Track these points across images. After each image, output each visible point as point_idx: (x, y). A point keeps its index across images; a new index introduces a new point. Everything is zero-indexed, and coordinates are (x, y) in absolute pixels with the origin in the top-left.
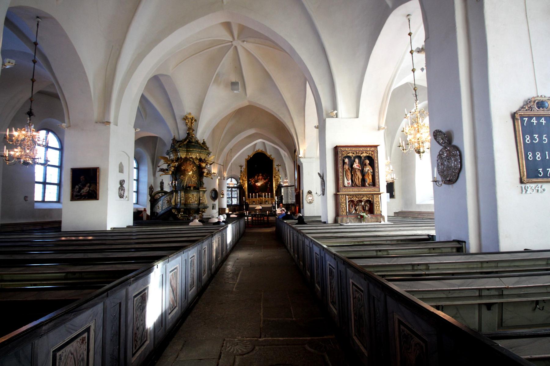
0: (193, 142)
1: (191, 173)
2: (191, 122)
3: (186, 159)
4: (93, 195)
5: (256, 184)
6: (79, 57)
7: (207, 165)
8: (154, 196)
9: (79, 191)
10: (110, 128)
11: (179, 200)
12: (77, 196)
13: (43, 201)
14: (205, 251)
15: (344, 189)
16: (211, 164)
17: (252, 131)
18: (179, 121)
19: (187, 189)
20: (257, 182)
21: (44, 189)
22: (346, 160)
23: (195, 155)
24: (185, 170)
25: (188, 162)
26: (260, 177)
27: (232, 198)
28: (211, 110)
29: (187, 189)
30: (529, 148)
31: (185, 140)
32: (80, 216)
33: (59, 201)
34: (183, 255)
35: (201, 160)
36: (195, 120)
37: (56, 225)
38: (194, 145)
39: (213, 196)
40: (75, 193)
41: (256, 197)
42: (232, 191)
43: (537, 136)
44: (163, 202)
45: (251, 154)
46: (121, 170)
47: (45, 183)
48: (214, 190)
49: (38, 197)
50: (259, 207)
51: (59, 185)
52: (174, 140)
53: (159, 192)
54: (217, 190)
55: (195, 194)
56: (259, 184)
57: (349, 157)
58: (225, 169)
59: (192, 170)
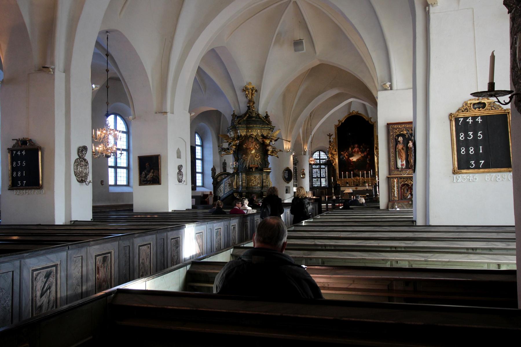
0: (253, 117)
1: (253, 152)
2: (251, 93)
3: (247, 137)
4: (156, 180)
5: (351, 159)
6: (139, 57)
7: (271, 141)
8: (217, 178)
9: (145, 177)
10: (166, 118)
11: (240, 183)
12: (144, 181)
13: (116, 185)
14: (234, 228)
15: (396, 172)
16: (276, 140)
17: (335, 92)
18: (239, 93)
19: (248, 171)
20: (352, 156)
21: (116, 173)
22: (400, 139)
23: (256, 132)
24: (247, 149)
25: (250, 140)
26: (356, 149)
27: (321, 178)
28: (274, 78)
29: (248, 171)
30: (466, 144)
31: (245, 114)
32: (145, 199)
33: (128, 185)
34: (208, 225)
35: (264, 137)
36: (256, 91)
37: (130, 207)
38: (253, 121)
39: (287, 177)
40: (142, 179)
41: (350, 177)
42: (320, 168)
43: (471, 133)
44: (225, 186)
45: (342, 117)
46: (179, 157)
47: (116, 167)
48: (288, 170)
49: (111, 182)
50: (349, 190)
51: (128, 168)
52: (234, 115)
53: (221, 175)
54: (292, 169)
55: (258, 176)
56: (354, 159)
57: (403, 136)
58: (305, 141)
59: (255, 148)
